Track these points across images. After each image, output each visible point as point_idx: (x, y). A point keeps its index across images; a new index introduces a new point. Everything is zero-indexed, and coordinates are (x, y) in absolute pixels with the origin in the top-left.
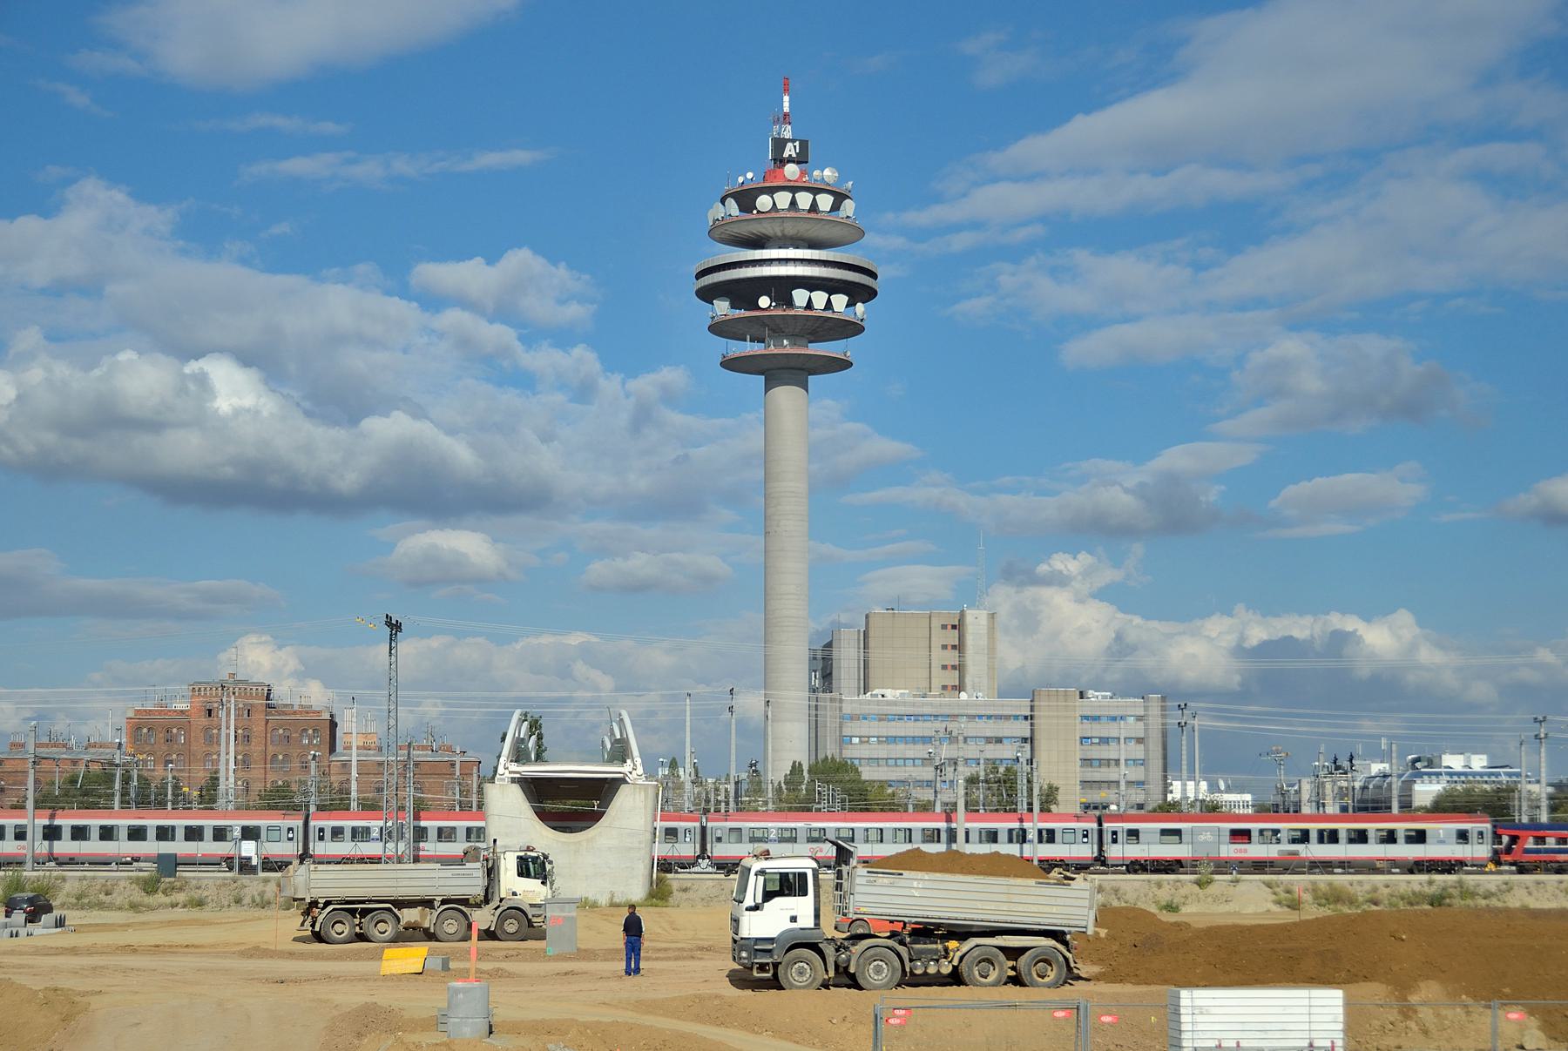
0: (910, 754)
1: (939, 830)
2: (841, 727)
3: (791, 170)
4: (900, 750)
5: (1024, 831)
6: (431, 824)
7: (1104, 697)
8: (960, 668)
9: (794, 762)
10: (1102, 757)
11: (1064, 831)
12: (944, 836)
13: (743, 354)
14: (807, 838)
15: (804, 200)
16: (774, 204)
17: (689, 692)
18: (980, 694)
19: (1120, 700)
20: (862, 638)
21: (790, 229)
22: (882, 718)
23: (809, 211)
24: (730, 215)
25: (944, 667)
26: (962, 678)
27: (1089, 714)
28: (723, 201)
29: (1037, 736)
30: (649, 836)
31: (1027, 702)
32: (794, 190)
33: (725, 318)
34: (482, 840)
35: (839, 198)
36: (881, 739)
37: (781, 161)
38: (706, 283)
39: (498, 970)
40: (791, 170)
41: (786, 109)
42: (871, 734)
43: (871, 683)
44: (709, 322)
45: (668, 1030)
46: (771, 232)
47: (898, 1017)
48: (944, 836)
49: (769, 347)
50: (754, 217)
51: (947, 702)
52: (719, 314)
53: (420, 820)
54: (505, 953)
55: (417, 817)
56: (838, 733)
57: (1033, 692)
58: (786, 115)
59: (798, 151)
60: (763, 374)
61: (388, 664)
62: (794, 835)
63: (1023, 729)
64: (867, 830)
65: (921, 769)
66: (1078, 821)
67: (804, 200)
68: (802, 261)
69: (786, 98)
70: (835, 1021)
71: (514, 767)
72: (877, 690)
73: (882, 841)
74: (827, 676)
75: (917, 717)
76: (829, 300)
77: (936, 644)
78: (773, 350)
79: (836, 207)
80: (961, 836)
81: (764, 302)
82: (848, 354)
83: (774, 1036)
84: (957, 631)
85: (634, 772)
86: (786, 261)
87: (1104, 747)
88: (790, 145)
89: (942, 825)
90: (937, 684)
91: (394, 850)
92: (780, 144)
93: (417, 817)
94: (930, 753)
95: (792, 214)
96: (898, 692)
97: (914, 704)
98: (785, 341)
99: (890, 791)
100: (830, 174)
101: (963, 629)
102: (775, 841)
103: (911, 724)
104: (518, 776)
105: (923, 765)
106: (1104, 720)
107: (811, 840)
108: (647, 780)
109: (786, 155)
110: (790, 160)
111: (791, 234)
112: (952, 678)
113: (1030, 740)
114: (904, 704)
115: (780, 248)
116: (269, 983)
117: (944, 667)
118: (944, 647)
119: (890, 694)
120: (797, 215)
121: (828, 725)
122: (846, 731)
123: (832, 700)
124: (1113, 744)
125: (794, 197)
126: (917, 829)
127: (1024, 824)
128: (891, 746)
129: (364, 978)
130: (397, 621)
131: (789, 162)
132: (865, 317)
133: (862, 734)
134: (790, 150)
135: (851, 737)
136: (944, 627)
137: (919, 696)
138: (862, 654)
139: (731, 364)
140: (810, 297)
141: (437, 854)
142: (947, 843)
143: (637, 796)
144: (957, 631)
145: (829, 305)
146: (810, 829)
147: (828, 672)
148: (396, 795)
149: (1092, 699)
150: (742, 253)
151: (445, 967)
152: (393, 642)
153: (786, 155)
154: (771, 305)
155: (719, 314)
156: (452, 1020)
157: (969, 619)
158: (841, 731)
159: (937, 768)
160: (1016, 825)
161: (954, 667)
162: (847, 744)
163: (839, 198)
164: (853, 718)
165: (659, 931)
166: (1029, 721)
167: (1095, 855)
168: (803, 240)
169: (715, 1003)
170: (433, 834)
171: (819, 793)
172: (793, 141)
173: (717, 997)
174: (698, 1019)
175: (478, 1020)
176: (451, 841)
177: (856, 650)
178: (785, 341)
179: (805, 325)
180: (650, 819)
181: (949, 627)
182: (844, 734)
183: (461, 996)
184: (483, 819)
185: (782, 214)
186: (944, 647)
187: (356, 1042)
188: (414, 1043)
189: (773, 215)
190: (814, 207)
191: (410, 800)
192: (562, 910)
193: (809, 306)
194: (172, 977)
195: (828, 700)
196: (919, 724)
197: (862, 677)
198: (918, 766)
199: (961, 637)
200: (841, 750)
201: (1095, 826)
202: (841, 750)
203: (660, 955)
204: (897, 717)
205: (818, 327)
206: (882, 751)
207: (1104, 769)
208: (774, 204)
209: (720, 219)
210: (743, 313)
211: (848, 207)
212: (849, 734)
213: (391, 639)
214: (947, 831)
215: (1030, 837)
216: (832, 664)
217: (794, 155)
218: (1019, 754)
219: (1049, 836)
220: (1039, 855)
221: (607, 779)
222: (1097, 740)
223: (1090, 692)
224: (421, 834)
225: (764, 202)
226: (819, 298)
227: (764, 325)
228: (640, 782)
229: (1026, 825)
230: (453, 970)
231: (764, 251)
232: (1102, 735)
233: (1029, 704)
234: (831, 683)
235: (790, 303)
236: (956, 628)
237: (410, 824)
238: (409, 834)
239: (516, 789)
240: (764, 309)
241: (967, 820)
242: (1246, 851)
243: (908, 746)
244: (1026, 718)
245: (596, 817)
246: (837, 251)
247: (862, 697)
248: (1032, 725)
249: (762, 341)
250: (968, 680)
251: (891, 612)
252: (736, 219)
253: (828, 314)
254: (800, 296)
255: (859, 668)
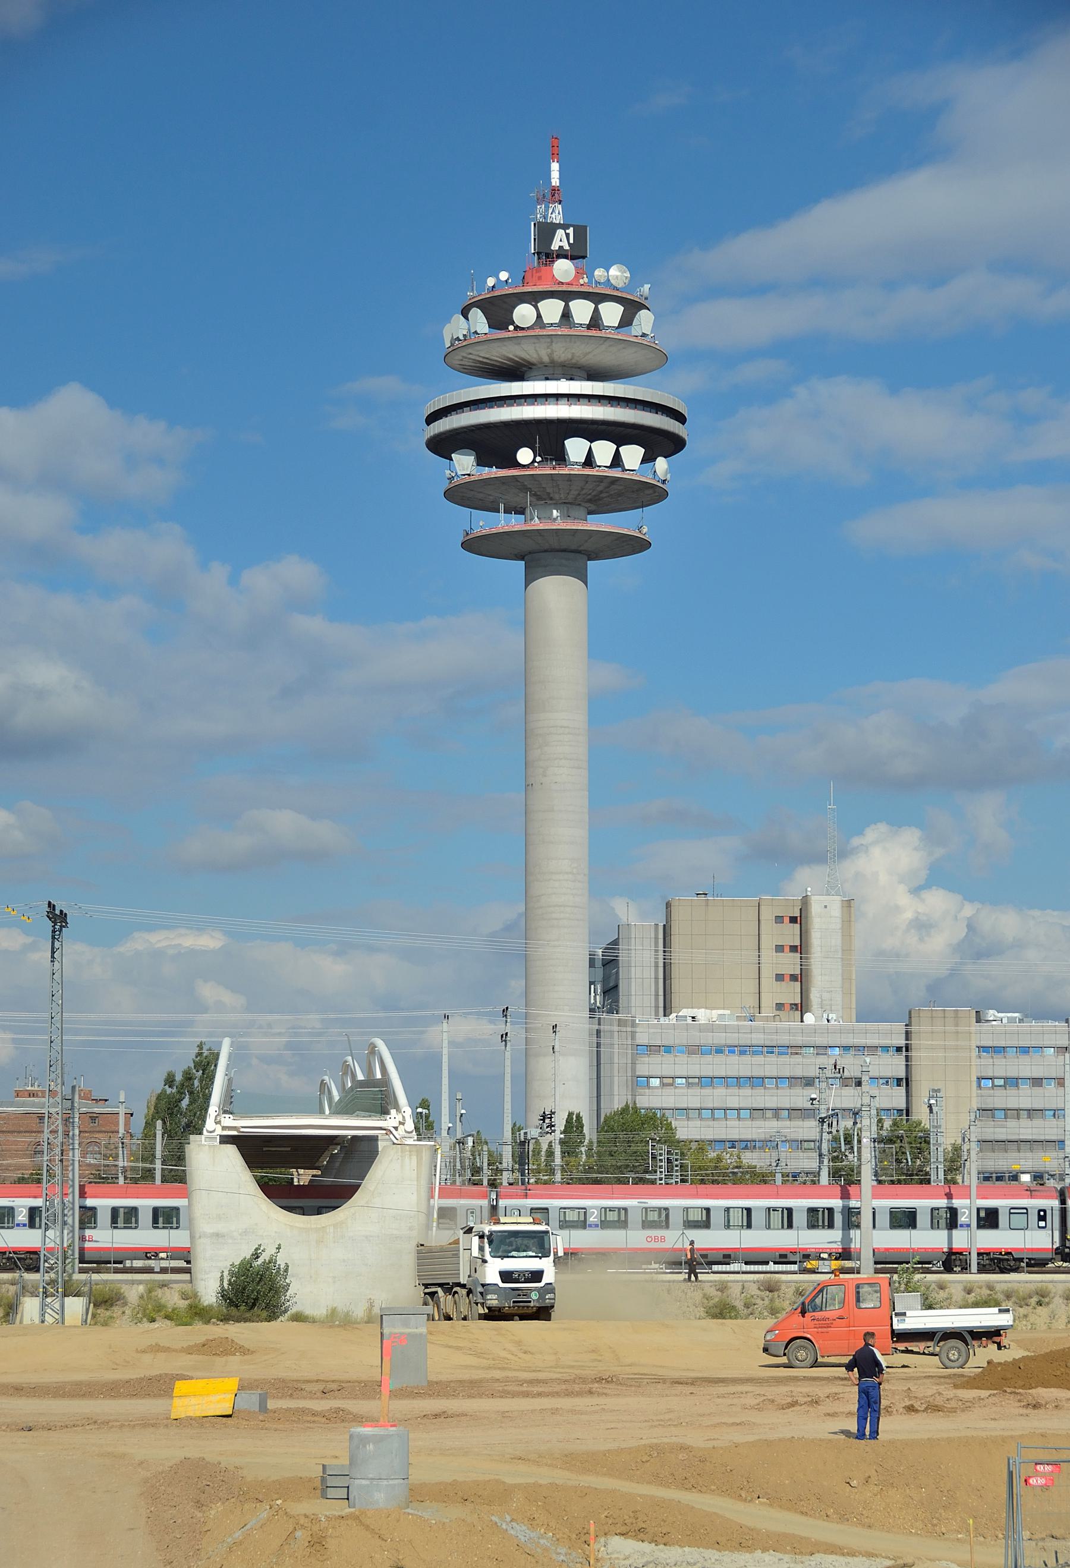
0: (733, 1102)
1: (831, 1210)
2: (634, 1063)
3: (563, 269)
4: (718, 1096)
5: (953, 1212)
6: (103, 1203)
7: (1011, 1020)
8: (801, 978)
9: (570, 1114)
10: (1009, 1106)
11: (1012, 1211)
12: (838, 1219)
13: (494, 531)
14: (684, 1221)
15: (582, 311)
16: (539, 316)
17: (447, 1013)
18: (833, 1016)
19: (1057, 1024)
20: (661, 936)
21: (562, 353)
22: (694, 1050)
23: (589, 327)
24: (476, 332)
25: (779, 977)
26: (804, 993)
27: (989, 1043)
28: (465, 313)
29: (915, 1076)
30: (422, 1218)
31: (900, 1027)
32: (567, 296)
33: (468, 479)
34: (175, 1225)
35: (632, 308)
36: (691, 1080)
37: (548, 256)
38: (436, 432)
39: (338, 1410)
40: (563, 269)
41: (555, 181)
42: (678, 1074)
43: (676, 1000)
44: (446, 485)
45: (640, 1496)
46: (535, 356)
47: (1043, 1475)
48: (838, 1219)
49: (532, 519)
50: (510, 335)
51: (787, 1030)
52: (459, 473)
53: (952, 1199)
54: (321, 1387)
55: (83, 1195)
56: (629, 1070)
57: (910, 1012)
58: (554, 190)
59: (571, 241)
60: (522, 559)
61: (50, 973)
62: (623, 1218)
63: (896, 1066)
64: (727, 1210)
65: (749, 1123)
66: (1032, 1197)
67: (582, 311)
68: (590, 398)
69: (555, 166)
70: (854, 1483)
71: (228, 1121)
72: (685, 1010)
73: (749, 1226)
74: (611, 991)
75: (743, 1050)
76: (617, 453)
77: (768, 943)
78: (537, 524)
79: (626, 321)
80: (866, 1219)
81: (525, 456)
82: (645, 530)
83: (771, 1505)
84: (797, 926)
85: (401, 1127)
86: (546, 397)
87: (1011, 1091)
88: (560, 233)
89: (836, 1203)
90: (768, 1002)
91: (58, 1241)
92: (546, 231)
93: (83, 1195)
94: (813, 1099)
95: (565, 331)
96: (715, 1013)
97: (738, 1030)
98: (555, 512)
99: (712, 1155)
100: (619, 274)
101: (807, 923)
102: (597, 1226)
103: (734, 1059)
104: (235, 1133)
105: (752, 1118)
106: (1011, 1052)
107: (647, 1225)
108: (419, 1140)
109: (555, 246)
110: (561, 254)
111: (562, 359)
112: (791, 993)
113: (906, 1082)
114: (725, 1029)
115: (547, 379)
116: (12, 1430)
117: (779, 977)
118: (780, 949)
119: (703, 1015)
120: (572, 332)
121: (616, 1060)
122: (642, 1070)
123: (620, 1022)
124: (1051, 1088)
125: (567, 307)
126: (800, 1208)
127: (954, 1201)
128: (707, 1091)
129: (148, 1423)
130: (61, 911)
131: (559, 256)
132: (668, 477)
133: (665, 1074)
134: (560, 240)
135: (649, 1077)
136: (779, 919)
137: (744, 1018)
138: (661, 953)
139: (475, 545)
140: (590, 447)
141: (800, 1246)
142: (843, 1230)
143: (407, 1160)
144: (797, 926)
145: (617, 461)
146: (646, 1209)
147: (612, 984)
148: (61, 1161)
149: (994, 1023)
150: (493, 386)
151: (263, 1407)
152: (56, 943)
153: (555, 246)
154: (534, 461)
155: (459, 473)
156: (357, 1482)
157: (816, 908)
158: (634, 1070)
159: (822, 1121)
160: (943, 1203)
161: (793, 978)
162: (642, 1087)
163: (632, 308)
164: (652, 1049)
165: (503, 1354)
166: (904, 1053)
167: (1057, 1245)
168: (580, 368)
169: (680, 1457)
170: (104, 1218)
171: (654, 1158)
172: (565, 227)
173: (683, 1448)
174: (657, 1479)
175: (396, 1482)
176: (131, 1228)
177: (653, 953)
178: (555, 512)
179: (582, 489)
180: (424, 1194)
181: (787, 920)
182: (638, 1073)
183: (371, 1447)
184: (185, 1194)
185: (549, 331)
186: (780, 949)
187: (199, 1515)
188: (306, 1516)
189: (538, 332)
190: (595, 322)
191: (73, 1170)
192: (406, 1325)
193: (589, 461)
194: (609, 1426)
195: (616, 1023)
196: (746, 1059)
197: (661, 992)
198: (745, 1119)
199: (804, 934)
200: (634, 1095)
201: (1056, 1203)
202: (634, 1095)
203: (536, 1389)
204: (765, 1049)
205: (601, 492)
206: (693, 1098)
207: (1012, 1123)
208: (539, 316)
209: (461, 338)
210: (494, 472)
211: (644, 321)
212: (647, 1074)
213: (53, 938)
214: (842, 1212)
215: (962, 1219)
216: (617, 973)
217: (567, 247)
218: (932, 1101)
219: (989, 1219)
220: (979, 1246)
221: (336, 1137)
222: (1002, 1082)
223: (991, 1012)
224: (88, 1217)
225: (524, 313)
226: (604, 451)
227: (525, 489)
228: (410, 1142)
229: (956, 1203)
230: (272, 1411)
231: (525, 384)
232: (1009, 1074)
233: (903, 1029)
234: (617, 1001)
235: (561, 457)
236: (796, 922)
237: (73, 1203)
238: (74, 1218)
239: (232, 1151)
240: (524, 466)
241: (875, 1196)
242: (663, 1239)
243: (730, 1091)
244: (899, 1049)
245: (346, 1192)
246: (618, 383)
247: (663, 1020)
248: (907, 1058)
249: (521, 511)
250: (814, 996)
251: (702, 898)
252: (484, 338)
253: (616, 473)
254: (576, 448)
255: (656, 978)
